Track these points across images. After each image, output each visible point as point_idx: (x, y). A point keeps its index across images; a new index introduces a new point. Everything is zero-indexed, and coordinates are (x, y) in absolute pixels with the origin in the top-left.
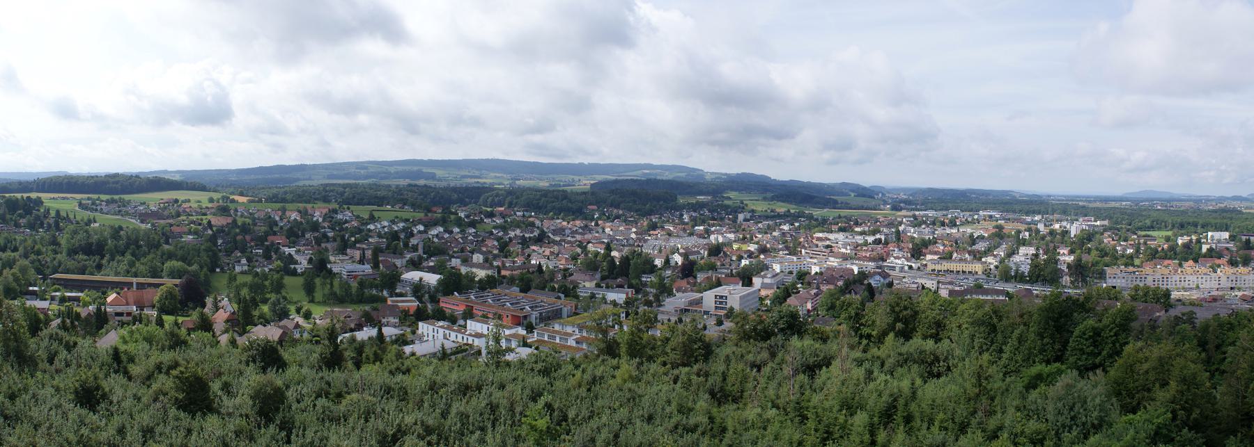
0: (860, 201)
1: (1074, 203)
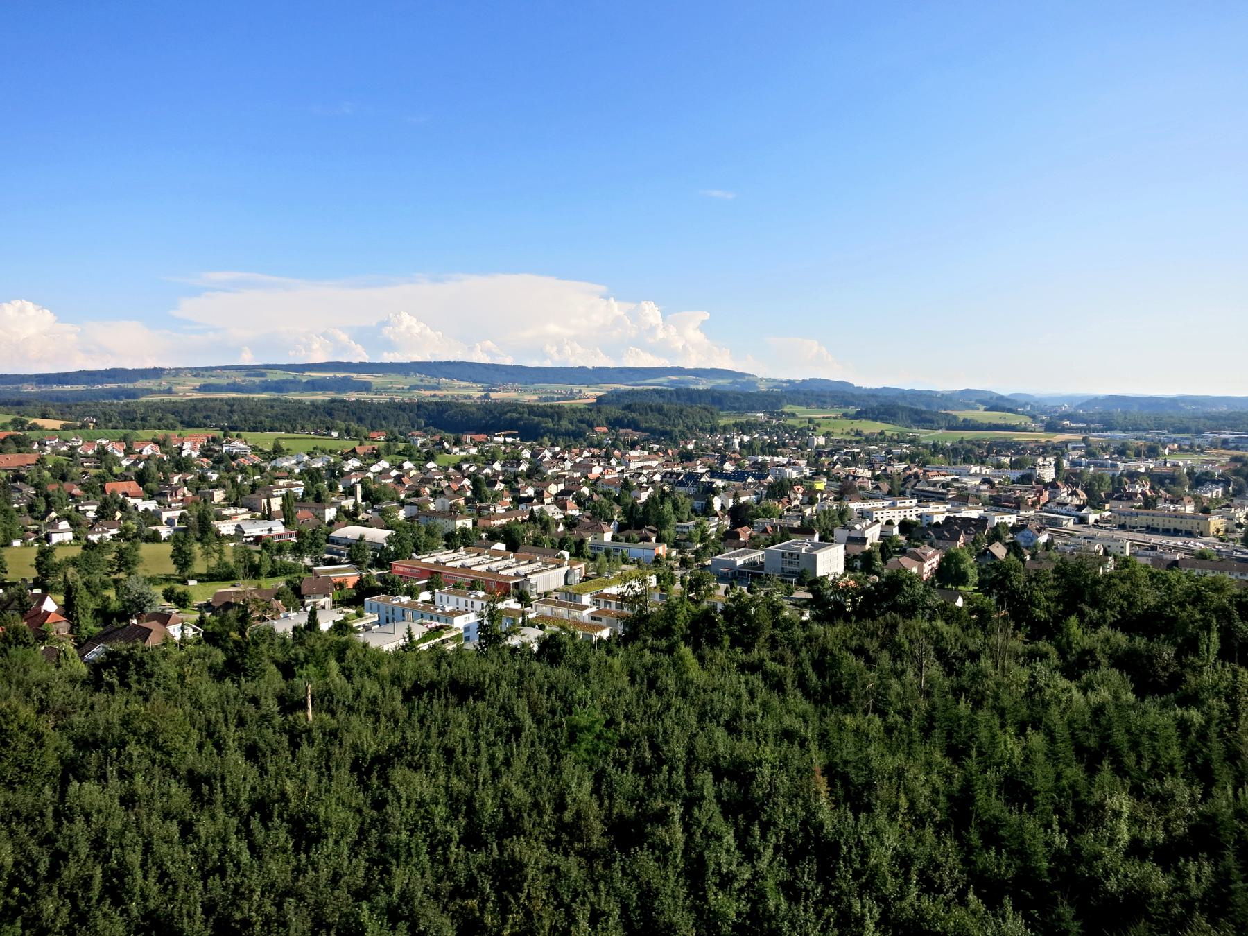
1: (352, 396)
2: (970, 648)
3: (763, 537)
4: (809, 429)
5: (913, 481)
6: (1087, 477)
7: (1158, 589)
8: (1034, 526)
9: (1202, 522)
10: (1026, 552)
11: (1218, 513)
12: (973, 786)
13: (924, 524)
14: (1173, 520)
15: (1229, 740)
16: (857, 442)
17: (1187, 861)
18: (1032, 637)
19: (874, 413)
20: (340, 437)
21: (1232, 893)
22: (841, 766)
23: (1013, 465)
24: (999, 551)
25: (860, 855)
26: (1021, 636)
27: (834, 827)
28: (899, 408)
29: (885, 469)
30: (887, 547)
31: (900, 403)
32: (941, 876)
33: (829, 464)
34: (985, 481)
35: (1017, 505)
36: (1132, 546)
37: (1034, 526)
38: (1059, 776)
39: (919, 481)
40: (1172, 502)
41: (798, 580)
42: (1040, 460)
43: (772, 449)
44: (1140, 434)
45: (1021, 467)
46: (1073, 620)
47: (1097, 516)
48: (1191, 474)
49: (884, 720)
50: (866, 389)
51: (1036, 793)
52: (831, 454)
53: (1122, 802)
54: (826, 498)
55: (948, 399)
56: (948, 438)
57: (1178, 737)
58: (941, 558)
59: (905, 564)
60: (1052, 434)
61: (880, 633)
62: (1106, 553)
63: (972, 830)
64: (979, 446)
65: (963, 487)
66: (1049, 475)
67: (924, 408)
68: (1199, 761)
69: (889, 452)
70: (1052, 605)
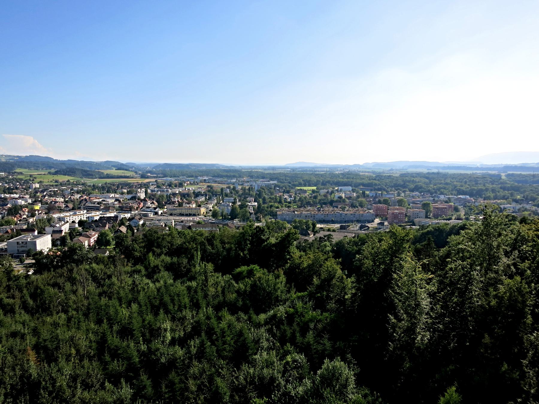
0: (120, 173)
2: (108, 274)
3: (6, 235)
4: (30, 180)
5: (84, 202)
6: (157, 196)
7: (181, 237)
8: (137, 217)
9: (198, 210)
10: (134, 228)
11: (204, 207)
12: (106, 335)
13: (90, 221)
14: (189, 210)
15: (205, 291)
16: (56, 186)
17: (191, 341)
18: (134, 264)
19: (64, 172)
20: (33, 179)
21: (205, 348)
22: (43, 343)
23: (128, 193)
24: (123, 229)
25: (51, 384)
26: (130, 264)
27: (38, 374)
28: (76, 169)
29: (71, 197)
30: (72, 233)
31: (77, 167)
32: (91, 380)
33: (42, 197)
34: (117, 200)
35: (130, 209)
36: (175, 222)
37: (137, 217)
38: (144, 321)
39: (87, 202)
40: (188, 204)
41: (27, 254)
42: (139, 190)
43: (10, 191)
44: (176, 178)
45: (132, 193)
46: (151, 254)
47: (162, 211)
48: (194, 193)
49: (67, 315)
50: (59, 161)
51: (134, 330)
52: (43, 192)
53: (168, 325)
54: (40, 213)
55: (100, 165)
56: (100, 182)
57: (188, 294)
58: (98, 235)
59: (81, 240)
60: (144, 179)
61: (65, 275)
62: (166, 225)
63: (106, 355)
64: (114, 185)
65: (107, 203)
66: (143, 196)
67: (88, 169)
68: (195, 301)
69: (72, 190)
70: (142, 249)
